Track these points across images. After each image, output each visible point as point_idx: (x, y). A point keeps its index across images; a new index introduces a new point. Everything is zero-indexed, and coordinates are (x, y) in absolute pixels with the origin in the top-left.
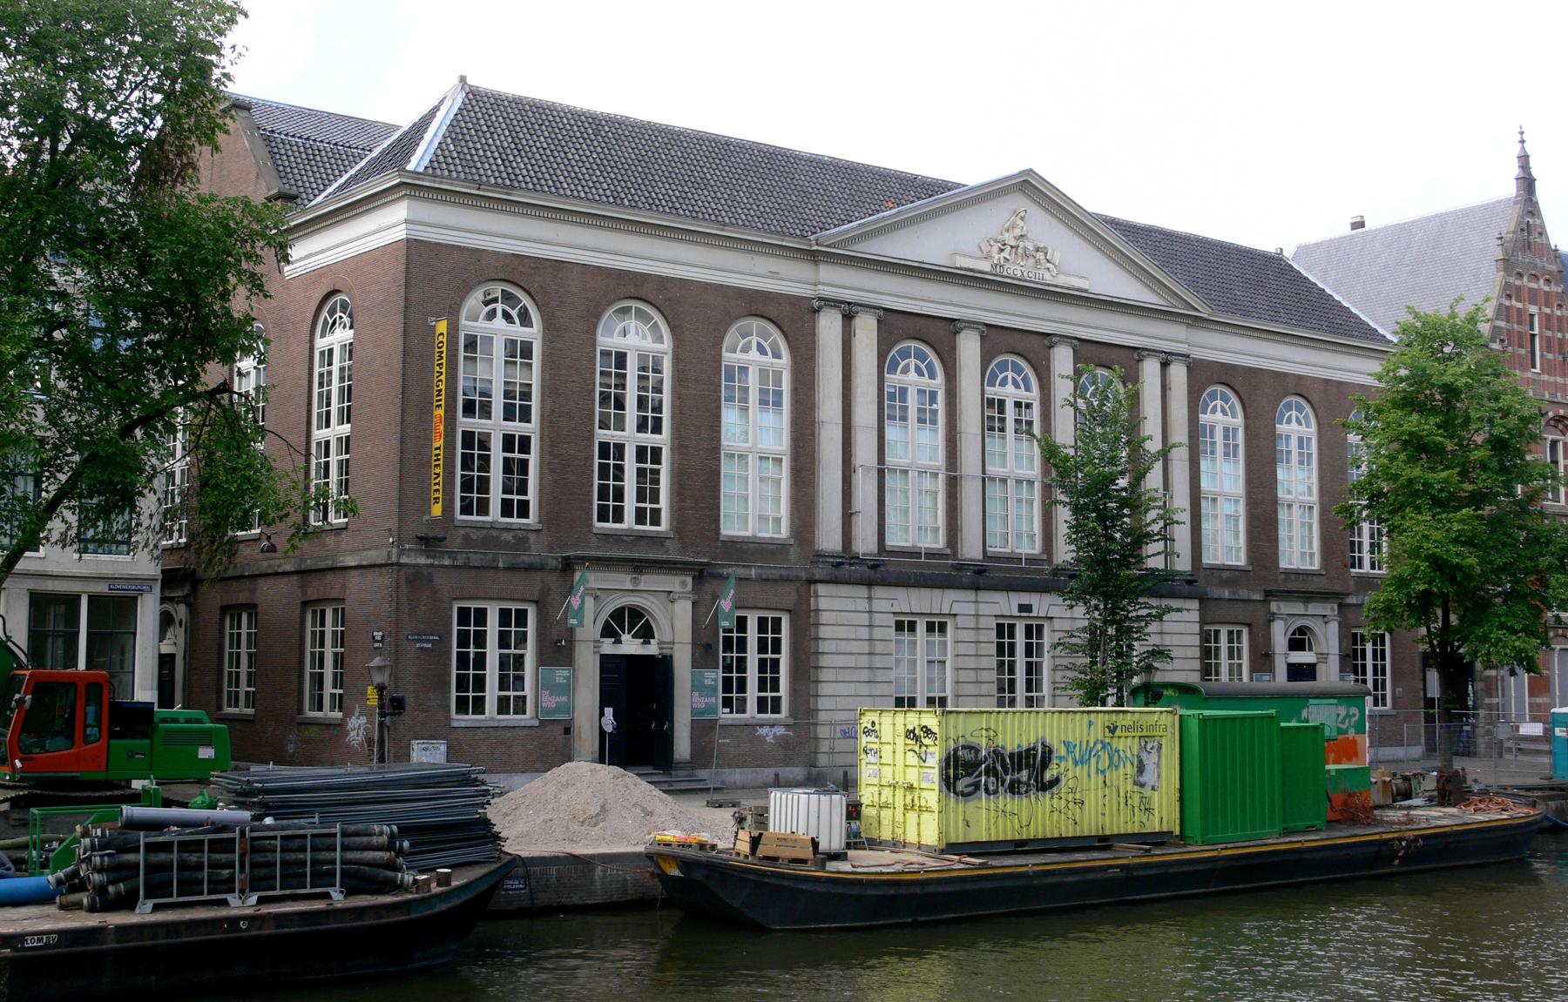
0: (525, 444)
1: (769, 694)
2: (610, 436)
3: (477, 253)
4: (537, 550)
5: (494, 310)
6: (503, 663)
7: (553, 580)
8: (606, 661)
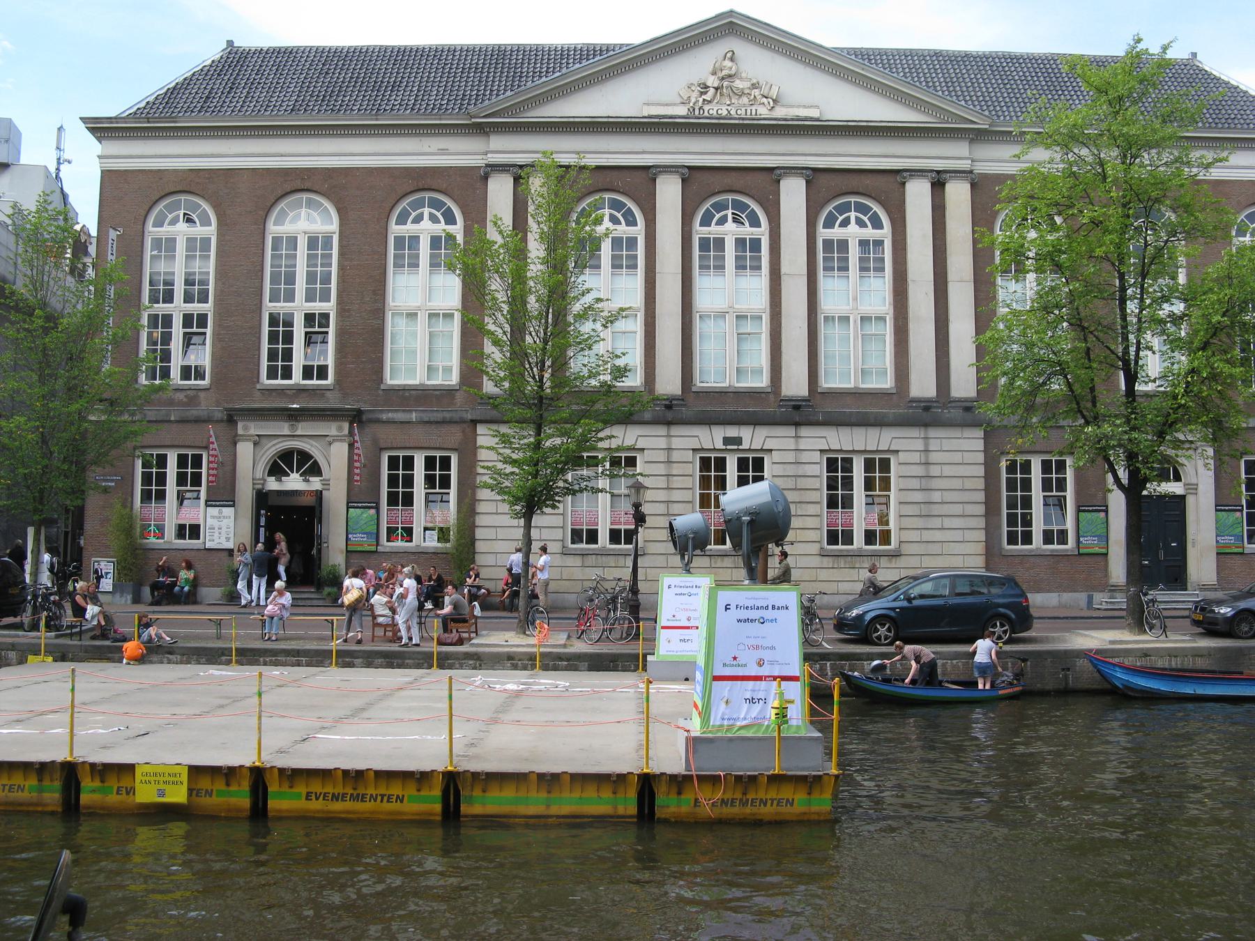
0: (202, 320)
1: (1055, 528)
2: (281, 307)
4: (207, 406)
5: (422, 214)
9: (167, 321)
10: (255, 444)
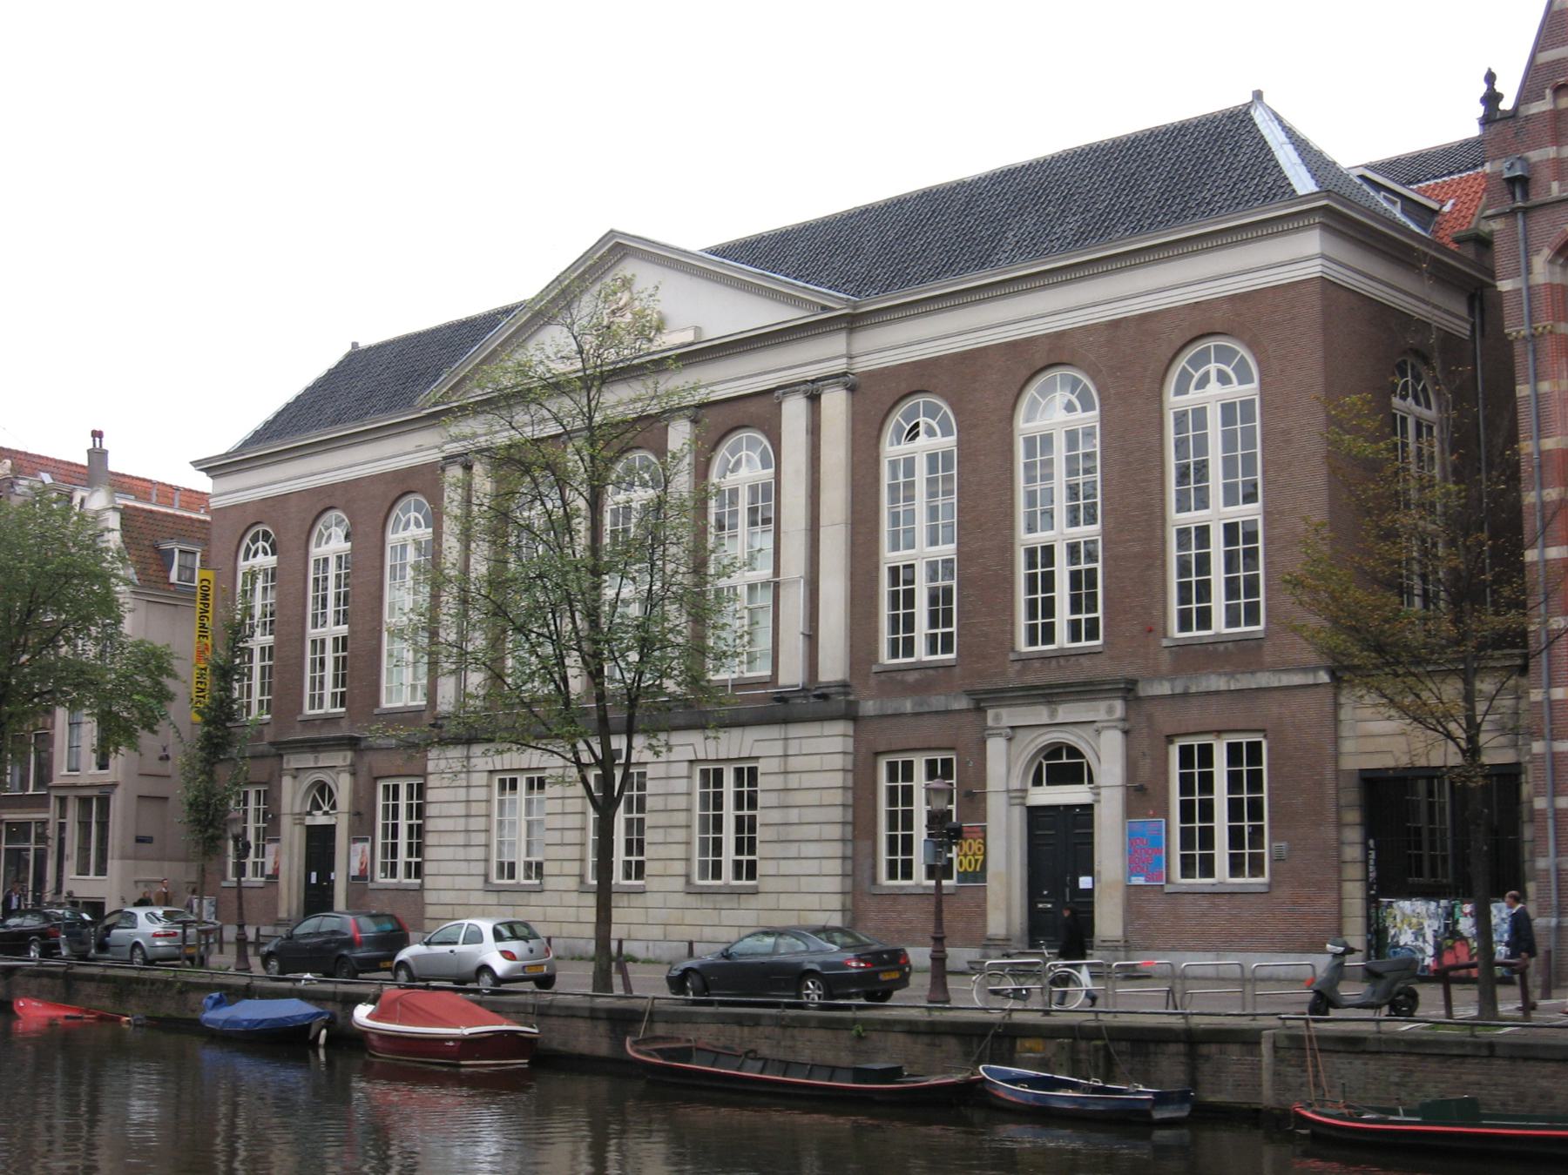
5: (1207, 374)
10: (1010, 739)
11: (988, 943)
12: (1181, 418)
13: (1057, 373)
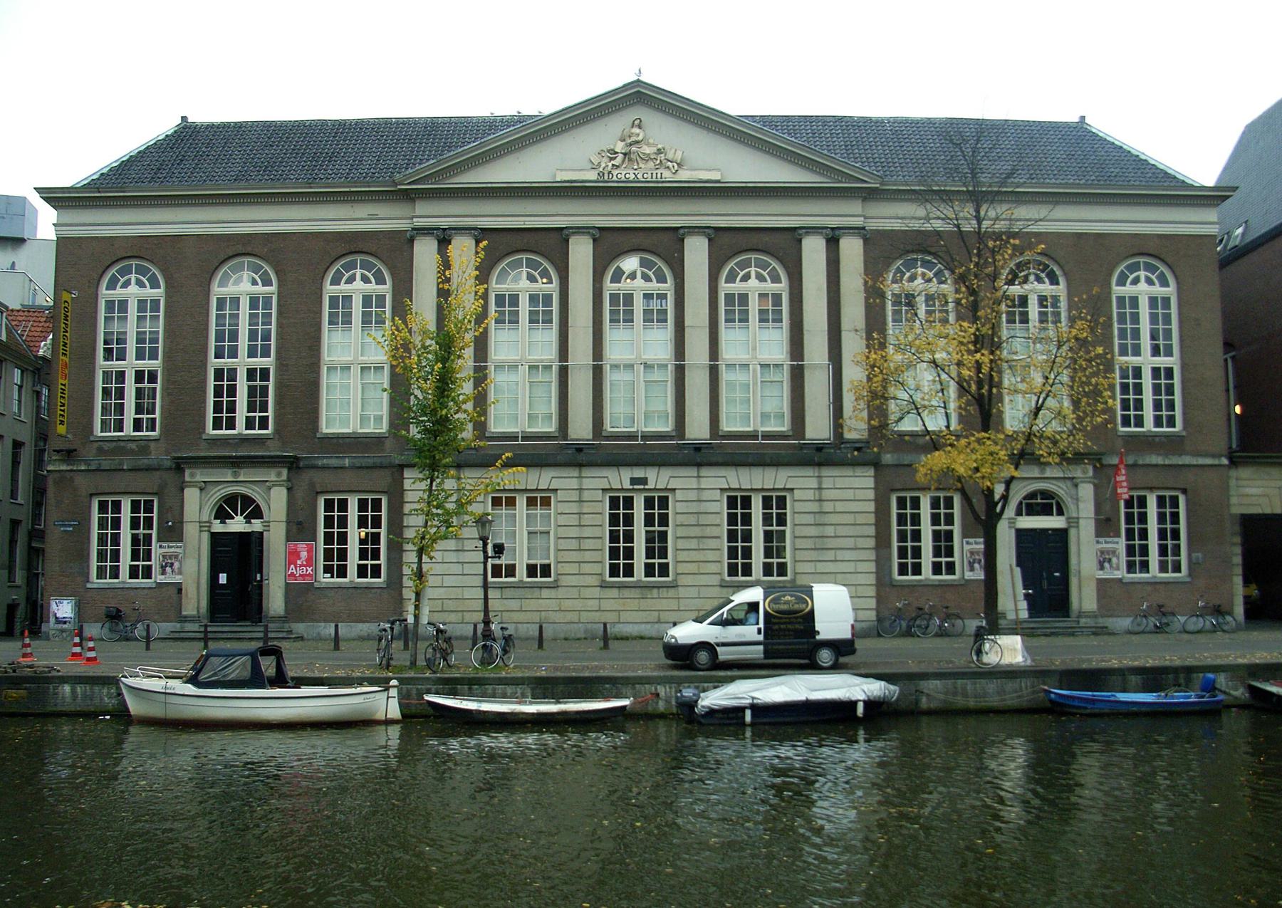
3: (111, 240)
4: (159, 455)
6: (650, 539)
7: (170, 477)
8: (216, 538)
9: (233, 373)
10: (201, 490)
11: (184, 619)
12: (221, 303)
13: (246, 260)
